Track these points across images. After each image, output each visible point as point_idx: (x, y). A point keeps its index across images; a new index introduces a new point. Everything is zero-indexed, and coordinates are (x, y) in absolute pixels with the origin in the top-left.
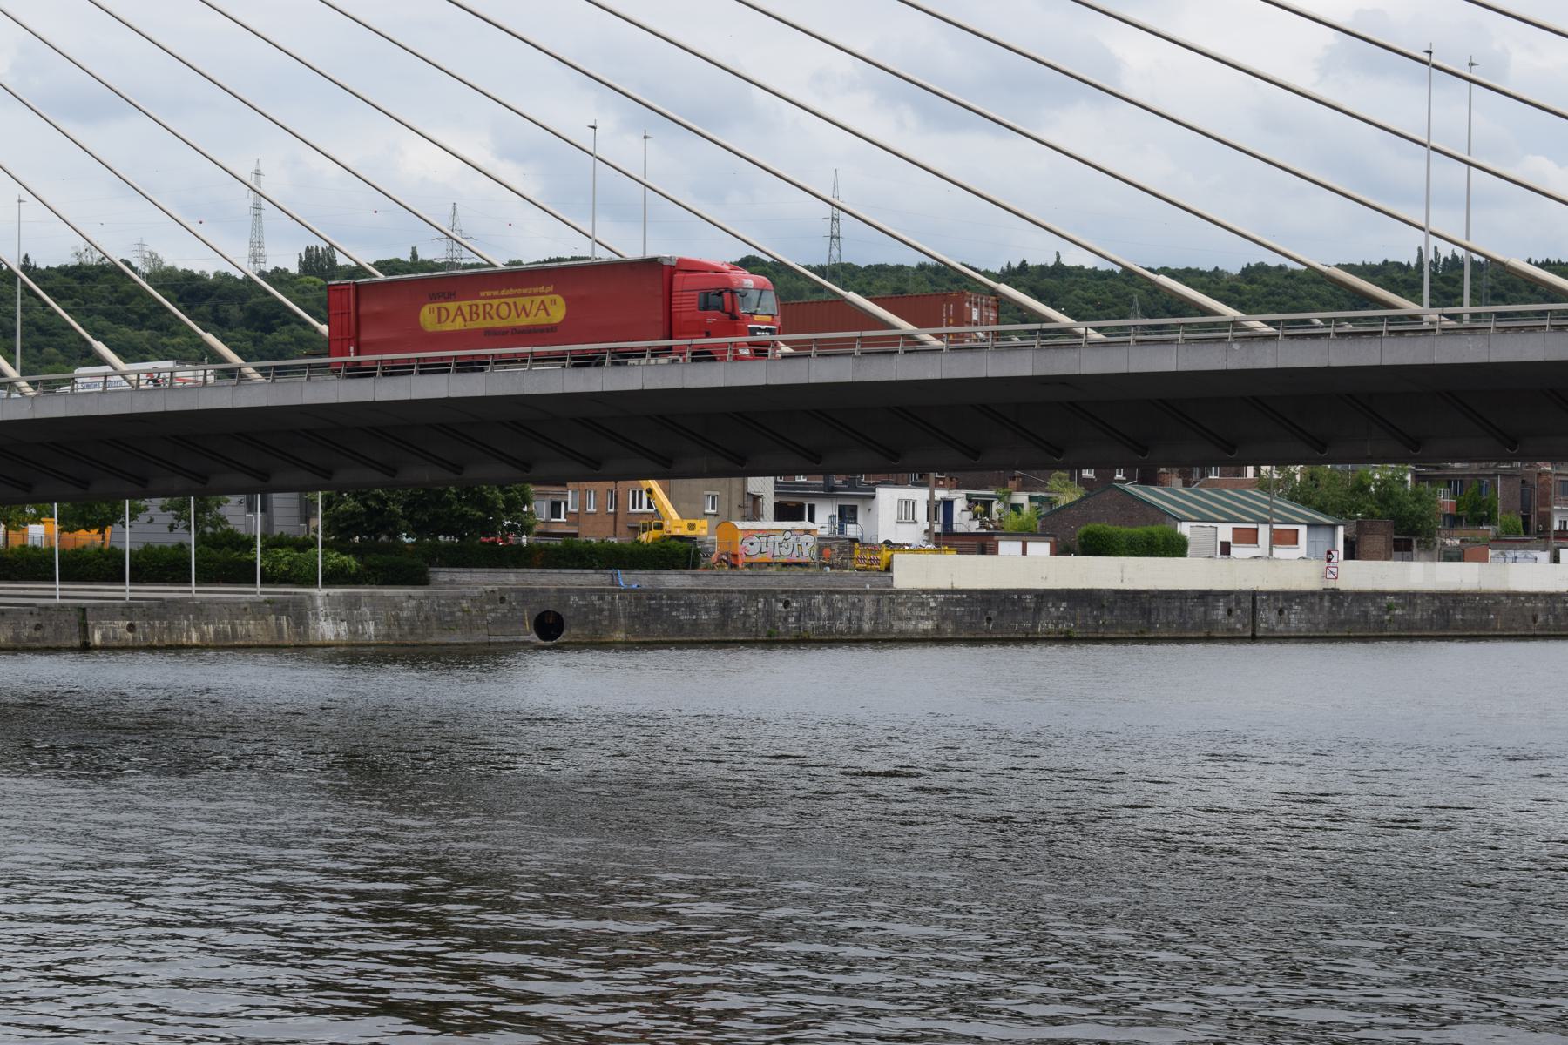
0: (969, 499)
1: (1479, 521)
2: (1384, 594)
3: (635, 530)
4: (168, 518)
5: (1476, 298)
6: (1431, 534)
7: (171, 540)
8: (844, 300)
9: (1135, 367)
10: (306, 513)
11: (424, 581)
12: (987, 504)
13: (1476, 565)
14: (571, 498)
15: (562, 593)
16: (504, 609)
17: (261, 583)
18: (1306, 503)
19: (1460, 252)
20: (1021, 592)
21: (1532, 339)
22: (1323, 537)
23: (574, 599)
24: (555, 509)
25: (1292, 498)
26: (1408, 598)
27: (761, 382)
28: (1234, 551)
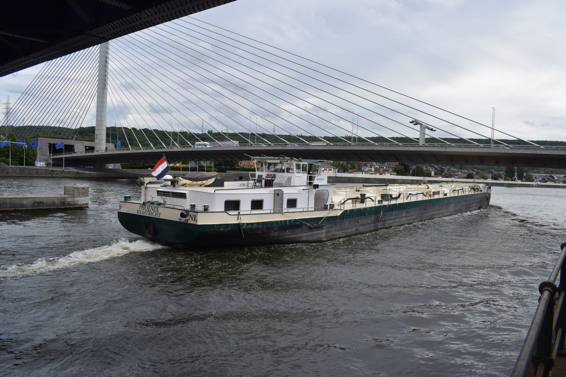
1: (353, 169)
2: (342, 177)
3: (251, 167)
4: (194, 163)
5: (358, 142)
6: (348, 170)
7: (195, 166)
8: (299, 139)
9: (354, 149)
10: (211, 163)
11: (225, 172)
13: (353, 174)
14: (243, 162)
15: (243, 174)
16: (235, 176)
17: (52, 166)
18: (333, 166)
19: (356, 136)
21: (365, 147)
22: (335, 170)
23: (244, 175)
24: (241, 163)
25: (331, 165)
26: (345, 178)
27: (549, 153)
28: (324, 171)
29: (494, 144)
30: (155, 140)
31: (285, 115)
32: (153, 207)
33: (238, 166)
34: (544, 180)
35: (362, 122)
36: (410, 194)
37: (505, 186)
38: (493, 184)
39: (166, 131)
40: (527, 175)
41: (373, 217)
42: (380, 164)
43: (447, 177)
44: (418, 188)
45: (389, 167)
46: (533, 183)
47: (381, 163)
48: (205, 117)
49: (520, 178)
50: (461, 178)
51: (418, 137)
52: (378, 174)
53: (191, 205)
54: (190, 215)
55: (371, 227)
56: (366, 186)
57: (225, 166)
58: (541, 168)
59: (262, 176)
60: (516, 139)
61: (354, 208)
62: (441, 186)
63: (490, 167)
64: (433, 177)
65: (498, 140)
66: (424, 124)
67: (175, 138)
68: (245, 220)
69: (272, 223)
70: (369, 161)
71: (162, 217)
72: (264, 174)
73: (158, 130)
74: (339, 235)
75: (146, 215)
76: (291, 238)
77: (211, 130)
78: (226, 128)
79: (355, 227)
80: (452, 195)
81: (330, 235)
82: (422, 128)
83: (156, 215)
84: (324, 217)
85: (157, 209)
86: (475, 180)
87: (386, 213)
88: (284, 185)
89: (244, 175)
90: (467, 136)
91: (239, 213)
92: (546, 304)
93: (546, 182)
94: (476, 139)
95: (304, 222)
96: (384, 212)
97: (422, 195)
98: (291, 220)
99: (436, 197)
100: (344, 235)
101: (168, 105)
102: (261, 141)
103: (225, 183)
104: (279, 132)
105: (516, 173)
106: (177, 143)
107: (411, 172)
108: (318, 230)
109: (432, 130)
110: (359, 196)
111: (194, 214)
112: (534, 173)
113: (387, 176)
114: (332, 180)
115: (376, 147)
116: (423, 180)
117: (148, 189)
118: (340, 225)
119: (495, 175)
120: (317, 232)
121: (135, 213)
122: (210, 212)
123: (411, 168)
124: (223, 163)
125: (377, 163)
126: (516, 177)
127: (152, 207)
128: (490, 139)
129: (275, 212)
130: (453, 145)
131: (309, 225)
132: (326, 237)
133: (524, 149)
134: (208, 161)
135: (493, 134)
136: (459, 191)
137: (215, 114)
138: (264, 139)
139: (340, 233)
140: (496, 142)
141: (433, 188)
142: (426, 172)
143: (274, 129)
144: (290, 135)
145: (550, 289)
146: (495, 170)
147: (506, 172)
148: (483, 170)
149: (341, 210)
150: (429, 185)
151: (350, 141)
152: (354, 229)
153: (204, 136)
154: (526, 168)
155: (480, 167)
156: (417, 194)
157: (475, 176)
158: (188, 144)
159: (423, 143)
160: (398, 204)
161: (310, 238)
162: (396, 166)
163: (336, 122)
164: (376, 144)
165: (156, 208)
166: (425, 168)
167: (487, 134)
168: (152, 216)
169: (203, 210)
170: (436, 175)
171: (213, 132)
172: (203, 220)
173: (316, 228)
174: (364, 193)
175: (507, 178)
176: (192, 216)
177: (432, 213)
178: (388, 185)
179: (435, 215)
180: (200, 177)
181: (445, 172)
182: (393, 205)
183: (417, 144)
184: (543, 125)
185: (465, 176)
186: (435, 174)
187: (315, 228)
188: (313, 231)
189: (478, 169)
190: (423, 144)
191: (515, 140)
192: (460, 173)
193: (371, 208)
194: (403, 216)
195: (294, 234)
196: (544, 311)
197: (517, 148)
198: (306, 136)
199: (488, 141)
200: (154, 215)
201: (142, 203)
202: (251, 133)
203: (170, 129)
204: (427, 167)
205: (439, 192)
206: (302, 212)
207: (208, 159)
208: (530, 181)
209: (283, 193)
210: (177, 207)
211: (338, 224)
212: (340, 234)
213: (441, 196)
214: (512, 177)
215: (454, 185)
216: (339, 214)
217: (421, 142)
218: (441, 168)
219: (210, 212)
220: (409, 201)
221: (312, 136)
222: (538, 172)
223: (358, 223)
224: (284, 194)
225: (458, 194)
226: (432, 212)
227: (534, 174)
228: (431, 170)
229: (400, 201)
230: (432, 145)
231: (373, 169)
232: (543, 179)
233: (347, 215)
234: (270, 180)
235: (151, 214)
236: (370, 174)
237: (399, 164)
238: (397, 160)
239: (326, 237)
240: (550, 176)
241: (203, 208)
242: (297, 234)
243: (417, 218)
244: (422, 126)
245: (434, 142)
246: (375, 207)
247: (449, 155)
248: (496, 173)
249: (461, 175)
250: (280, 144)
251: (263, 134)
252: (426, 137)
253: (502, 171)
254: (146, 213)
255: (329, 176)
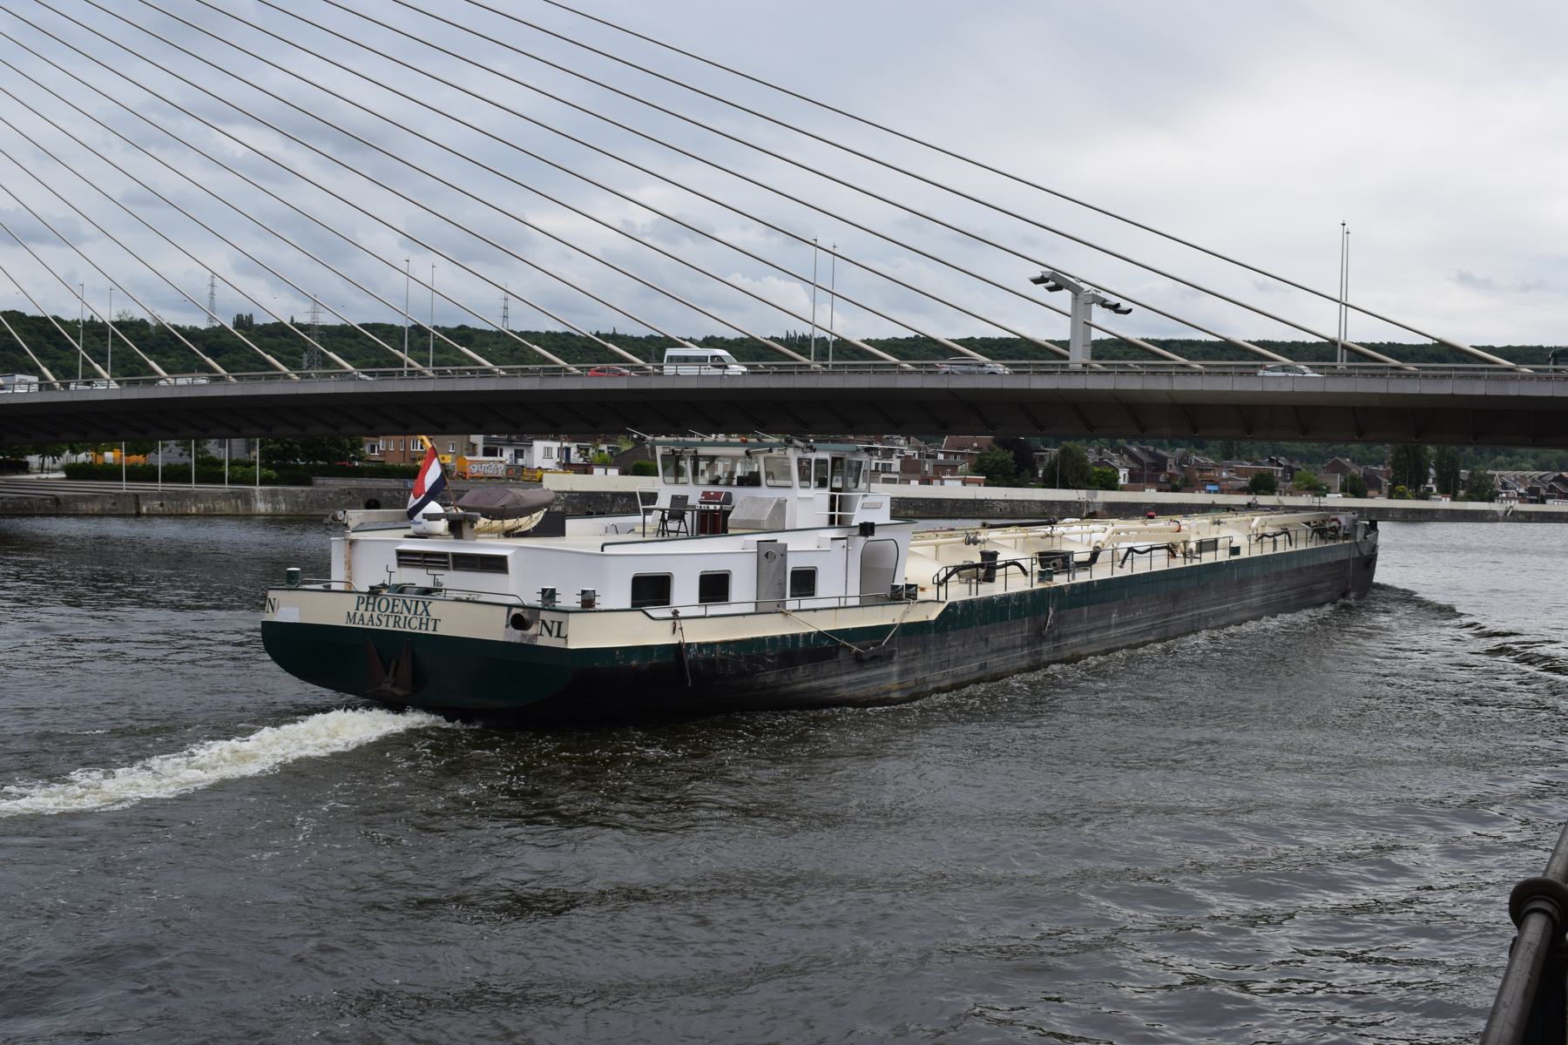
0: (578, 447)
3: (414, 460)
4: (179, 450)
7: (181, 461)
8: (606, 347)
10: (250, 448)
11: (310, 484)
12: (587, 450)
16: (350, 498)
19: (828, 336)
20: (605, 493)
23: (385, 494)
29: (1349, 360)
30: (10, 353)
31: (544, 255)
32: (409, 603)
33: (359, 460)
34: (1534, 495)
35: (851, 280)
36: (1131, 550)
37: (1393, 520)
38: (1384, 514)
39: (57, 319)
40: (1471, 475)
41: (1025, 628)
42: (922, 445)
43: (1175, 489)
44: (1150, 531)
45: (956, 455)
46: (1495, 506)
47: (927, 437)
48: (220, 259)
49: (1448, 488)
50: (1230, 491)
51: (1066, 336)
52: (915, 483)
53: (544, 591)
54: (544, 622)
55: (1022, 657)
56: (992, 527)
57: (307, 457)
58: (1522, 450)
59: (686, 498)
60: (1430, 342)
61: (974, 596)
62: (1219, 523)
63: (1335, 447)
64: (1123, 489)
65: (1362, 344)
66: (1086, 287)
67: (98, 345)
68: (695, 634)
69: (759, 642)
70: (878, 433)
71: (442, 631)
72: (694, 493)
73: (23, 315)
74: (934, 682)
75: (383, 627)
76: (811, 690)
77: (245, 314)
78: (308, 306)
79: (978, 655)
80: (1256, 552)
81: (910, 680)
82: (1081, 303)
83: (423, 627)
84: (894, 625)
85: (426, 607)
86: (1282, 498)
87: (1062, 612)
88: (765, 526)
89: (385, 494)
90: (1246, 330)
91: (676, 613)
92: (1533, 966)
93: (1544, 502)
94: (1283, 343)
95: (843, 642)
96: (1056, 611)
97: (1165, 552)
98: (810, 633)
99: (1208, 558)
100: (948, 682)
101: (61, 211)
102: (452, 356)
103: (571, 525)
104: (523, 321)
105: (1432, 471)
106: (106, 370)
107: (1041, 472)
108: (878, 667)
109: (1115, 308)
110: (978, 560)
111: (557, 617)
112: (1496, 467)
113: (951, 489)
114: (905, 510)
115: (907, 377)
116: (1088, 504)
117: (359, 548)
118: (937, 649)
119: (1354, 478)
120: (877, 672)
121: (341, 622)
122: (600, 611)
123: (1042, 458)
124: (298, 447)
125: (912, 438)
126: (1431, 484)
127: (404, 601)
128: (1333, 343)
129: (759, 611)
130: (1196, 365)
131: (855, 648)
132: (901, 689)
133: (1461, 377)
134: (234, 441)
135: (1343, 323)
136: (1277, 538)
137: (262, 248)
138: (464, 349)
139: (937, 677)
140: (1354, 354)
141: (1195, 528)
142: (1097, 469)
143: (506, 308)
144: (568, 334)
145: (1549, 908)
146: (1353, 460)
147: (1396, 465)
148: (1309, 459)
149: (938, 601)
150: (1184, 522)
151: (807, 354)
152: (975, 665)
153: (218, 337)
154: (1469, 450)
155: (1300, 447)
156: (1151, 549)
157: (1281, 483)
158: (153, 372)
159: (1086, 361)
160: (1098, 581)
161: (860, 692)
162: (986, 449)
163: (748, 280)
164: (906, 365)
165: (420, 604)
166: (1092, 457)
167: (1323, 323)
168: (408, 630)
169: (580, 605)
170: (1136, 481)
171: (258, 321)
172: (584, 635)
173: (874, 658)
174: (989, 548)
175: (1401, 488)
176: (549, 624)
177: (1196, 612)
178: (1055, 523)
179: (1206, 619)
180: (512, 507)
181: (1169, 470)
182: (1083, 585)
183: (1063, 365)
184: (1526, 288)
185: (1244, 482)
186: (1133, 477)
187: (871, 658)
188: (868, 669)
189: (1291, 456)
190: (1084, 365)
191: (1425, 346)
192: (1224, 474)
193: (1021, 596)
194: (1113, 621)
195: (815, 679)
196: (1526, 992)
197: (1435, 377)
198: (632, 337)
199: (1323, 352)
200: (414, 627)
201: (368, 590)
202: (410, 324)
203: (71, 311)
204: (1100, 452)
205: (1216, 541)
206: (836, 608)
207: (237, 433)
208: (1483, 500)
209: (786, 550)
210: (484, 598)
211: (932, 648)
212: (936, 678)
213: (1223, 556)
214: (1417, 488)
215: (1257, 519)
216: (933, 616)
217: (1078, 357)
218: (1152, 455)
219: (600, 611)
220: (1129, 573)
221: (657, 334)
222: (1511, 466)
223: (987, 645)
224: (788, 554)
225: (1275, 549)
226: (1198, 608)
227: (1497, 473)
228: (1116, 463)
229: (1101, 572)
230: (1119, 366)
231: (896, 464)
232: (1533, 491)
233: (957, 617)
234: (715, 511)
235: (401, 623)
236: (886, 481)
237: (995, 441)
238: (987, 427)
239: (901, 689)
240: (1555, 479)
241: (579, 599)
242: (825, 678)
243: (1153, 627)
244: (1081, 296)
245: (1126, 356)
246: (1033, 593)
247: (1182, 405)
248: (1357, 471)
249: (1226, 480)
250: (530, 367)
251: (462, 328)
252: (1096, 335)
253: (1382, 463)
254: (384, 620)
255: (894, 496)
